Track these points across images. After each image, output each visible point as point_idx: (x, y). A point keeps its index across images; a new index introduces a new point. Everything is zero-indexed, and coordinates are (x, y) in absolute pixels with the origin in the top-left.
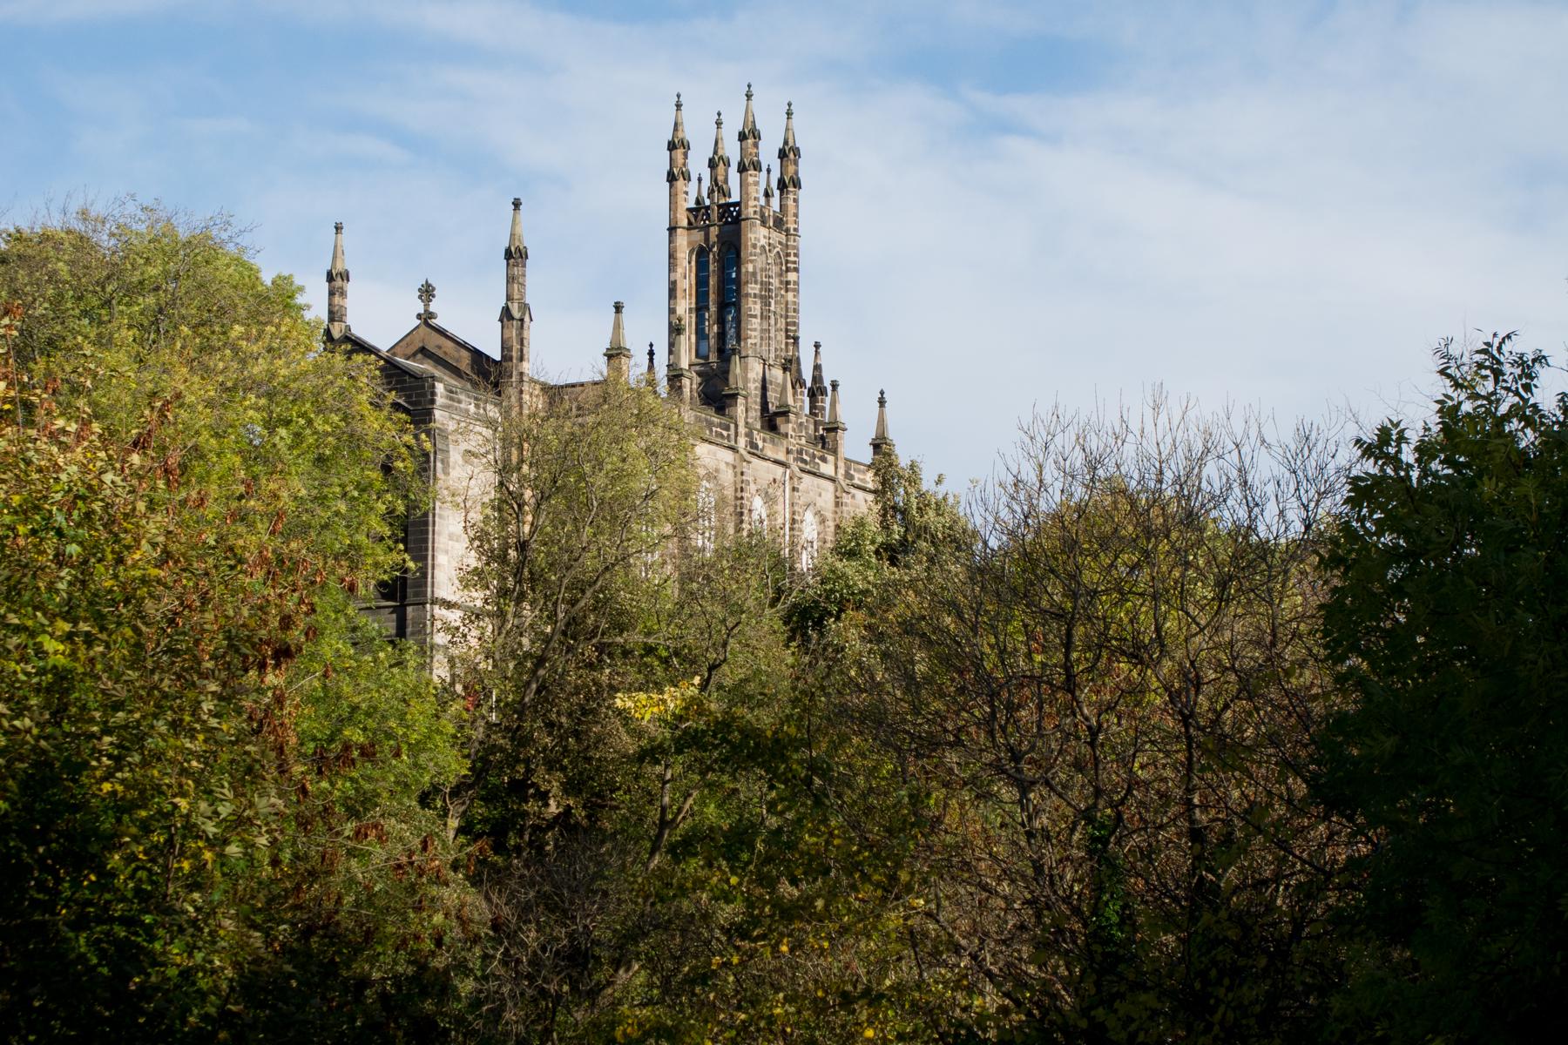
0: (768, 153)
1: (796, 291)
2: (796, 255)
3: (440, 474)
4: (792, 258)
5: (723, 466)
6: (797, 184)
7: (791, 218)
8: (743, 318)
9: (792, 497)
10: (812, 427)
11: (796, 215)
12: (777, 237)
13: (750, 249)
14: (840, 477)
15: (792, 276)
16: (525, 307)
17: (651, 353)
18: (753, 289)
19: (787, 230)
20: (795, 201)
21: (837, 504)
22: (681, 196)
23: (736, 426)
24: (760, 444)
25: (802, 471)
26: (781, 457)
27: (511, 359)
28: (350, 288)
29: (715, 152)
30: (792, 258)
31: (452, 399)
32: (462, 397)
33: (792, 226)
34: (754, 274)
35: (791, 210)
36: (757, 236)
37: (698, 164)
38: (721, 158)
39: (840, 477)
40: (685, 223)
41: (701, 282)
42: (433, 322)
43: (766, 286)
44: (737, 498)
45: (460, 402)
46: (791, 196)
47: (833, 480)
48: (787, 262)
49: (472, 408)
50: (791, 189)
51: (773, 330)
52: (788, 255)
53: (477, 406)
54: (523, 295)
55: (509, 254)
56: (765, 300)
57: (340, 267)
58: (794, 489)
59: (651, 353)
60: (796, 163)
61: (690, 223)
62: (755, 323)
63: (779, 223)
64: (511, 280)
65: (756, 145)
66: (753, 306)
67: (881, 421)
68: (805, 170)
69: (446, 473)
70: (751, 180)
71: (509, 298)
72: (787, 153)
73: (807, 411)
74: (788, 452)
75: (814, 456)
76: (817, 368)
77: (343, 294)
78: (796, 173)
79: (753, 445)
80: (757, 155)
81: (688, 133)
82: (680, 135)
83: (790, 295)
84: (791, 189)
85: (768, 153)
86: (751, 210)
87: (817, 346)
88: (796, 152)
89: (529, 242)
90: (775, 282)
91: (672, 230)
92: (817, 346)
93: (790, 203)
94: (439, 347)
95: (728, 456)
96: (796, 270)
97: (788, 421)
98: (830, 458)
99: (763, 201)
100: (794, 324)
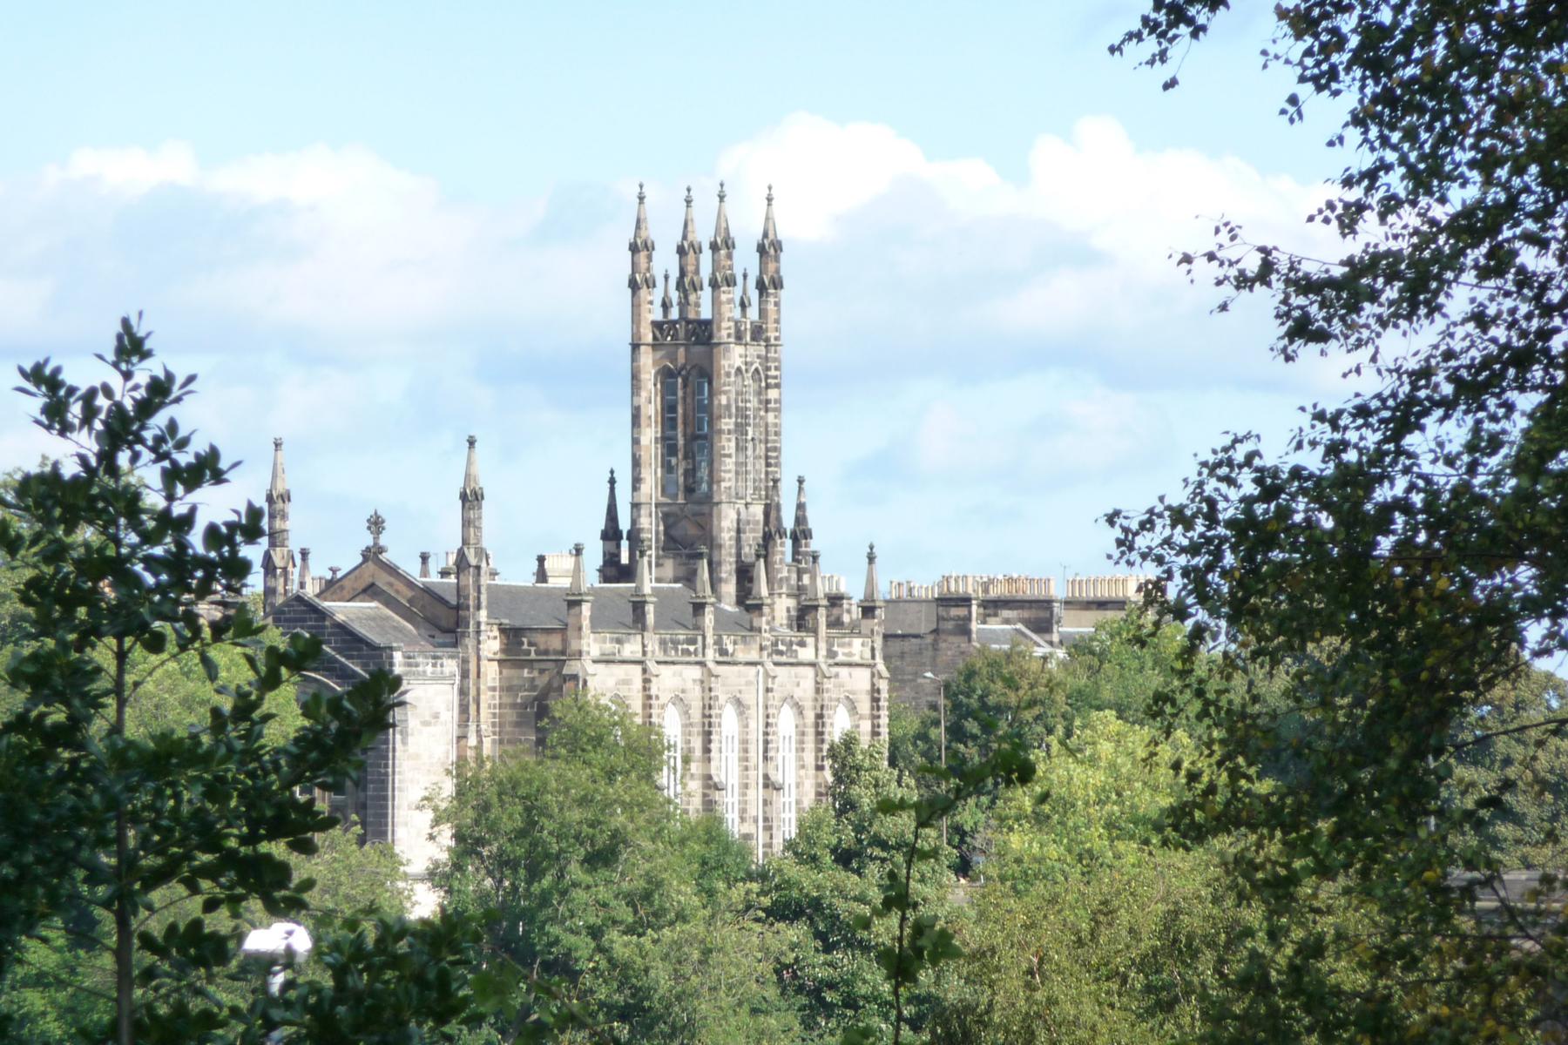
0: (745, 261)
1: (778, 410)
2: (777, 368)
3: (398, 745)
4: (772, 373)
5: (690, 685)
6: (778, 284)
7: (771, 325)
8: (716, 458)
9: (766, 699)
10: (794, 576)
11: (777, 321)
12: (756, 350)
13: (723, 379)
14: (821, 659)
15: (773, 394)
16: (482, 553)
17: (612, 482)
18: (727, 424)
19: (767, 340)
20: (777, 304)
21: (818, 691)
22: (645, 307)
23: (704, 638)
24: (730, 648)
25: (776, 664)
26: (754, 655)
27: (468, 608)
28: (291, 508)
29: (685, 237)
30: (772, 373)
31: (410, 665)
32: (420, 660)
33: (772, 335)
34: (728, 407)
35: (772, 316)
36: (734, 357)
37: (665, 262)
38: (692, 245)
39: (821, 659)
40: (649, 338)
41: (668, 408)
42: (384, 557)
43: (742, 413)
44: (704, 716)
45: (417, 665)
46: (772, 299)
47: (813, 665)
48: (765, 378)
49: (429, 669)
50: (771, 291)
51: (750, 460)
52: (768, 369)
53: (434, 665)
54: (479, 540)
55: (464, 497)
56: (740, 429)
57: (280, 488)
58: (768, 690)
59: (612, 482)
60: (777, 259)
61: (655, 338)
62: (729, 464)
63: (758, 333)
64: (467, 523)
65: (729, 257)
66: (728, 444)
67: (870, 581)
68: (788, 265)
69: (404, 743)
70: (724, 297)
71: (465, 542)
72: (768, 249)
73: (789, 558)
74: (762, 648)
75: (791, 643)
76: (801, 507)
77: (284, 517)
78: (777, 271)
79: (723, 652)
80: (731, 268)
81: (653, 232)
82: (643, 234)
83: (771, 417)
84: (771, 291)
85: (745, 261)
86: (724, 333)
87: (801, 481)
88: (777, 246)
89: (485, 482)
90: (753, 403)
91: (635, 347)
92: (801, 481)
93: (771, 307)
94: (391, 585)
95: (695, 672)
96: (777, 386)
97: (761, 615)
98: (810, 640)
99: (737, 313)
100: (775, 449)
